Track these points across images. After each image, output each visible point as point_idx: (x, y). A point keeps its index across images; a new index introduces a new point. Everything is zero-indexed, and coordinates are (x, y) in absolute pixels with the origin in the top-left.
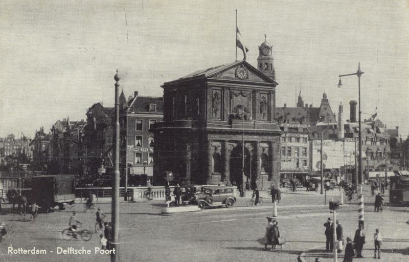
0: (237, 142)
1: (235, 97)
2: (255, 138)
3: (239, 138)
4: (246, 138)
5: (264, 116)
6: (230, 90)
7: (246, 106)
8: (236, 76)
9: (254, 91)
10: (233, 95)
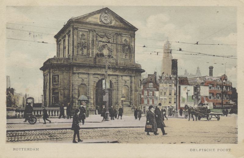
5: (126, 55)
10: (98, 36)
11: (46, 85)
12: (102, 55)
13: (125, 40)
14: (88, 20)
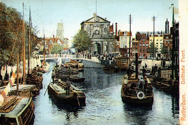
0: (96, 41)
1: (95, 27)
7: (99, 30)
13: (106, 27)
14: (89, 21)
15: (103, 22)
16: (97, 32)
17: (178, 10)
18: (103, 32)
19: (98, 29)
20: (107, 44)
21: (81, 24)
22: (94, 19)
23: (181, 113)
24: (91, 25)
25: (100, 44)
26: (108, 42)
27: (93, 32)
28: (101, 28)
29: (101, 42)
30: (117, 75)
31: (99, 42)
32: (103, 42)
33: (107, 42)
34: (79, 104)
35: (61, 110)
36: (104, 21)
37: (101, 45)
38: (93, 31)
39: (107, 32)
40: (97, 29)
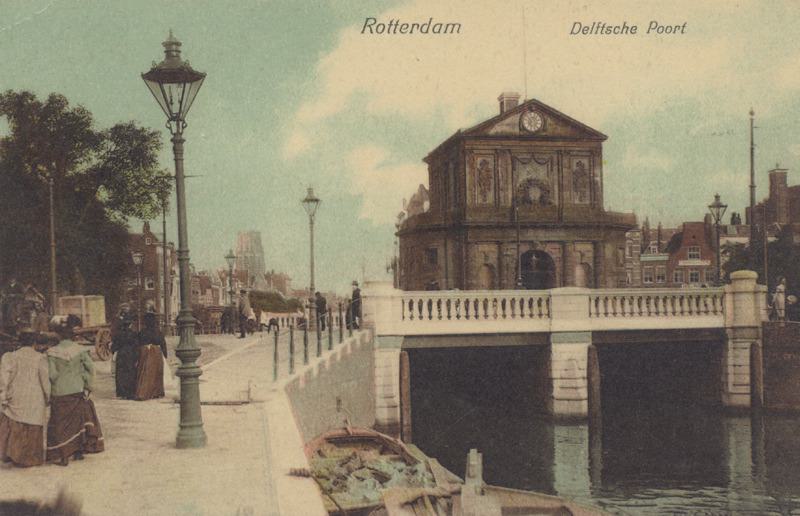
2: (561, 235)
3: (530, 235)
4: (542, 235)
6: (510, 153)
8: (522, 128)
9: (559, 152)
11: (467, 257)
12: (526, 200)
14: (492, 132)
15: (564, 138)
16: (535, 194)
17: (207, 333)
18: (566, 194)
19: (541, 173)
20: (493, 260)
21: (425, 160)
22: (517, 122)
23: (397, 510)
24: (504, 152)
25: (554, 257)
26: (595, 244)
27: (510, 191)
28: (555, 168)
29: (557, 246)
30: (344, 432)
31: (548, 249)
32: (570, 248)
33: (589, 247)
34: (75, 436)
35: (47, 404)
36: (569, 129)
37: (558, 265)
38: (510, 186)
39: (588, 193)
40: (533, 176)
